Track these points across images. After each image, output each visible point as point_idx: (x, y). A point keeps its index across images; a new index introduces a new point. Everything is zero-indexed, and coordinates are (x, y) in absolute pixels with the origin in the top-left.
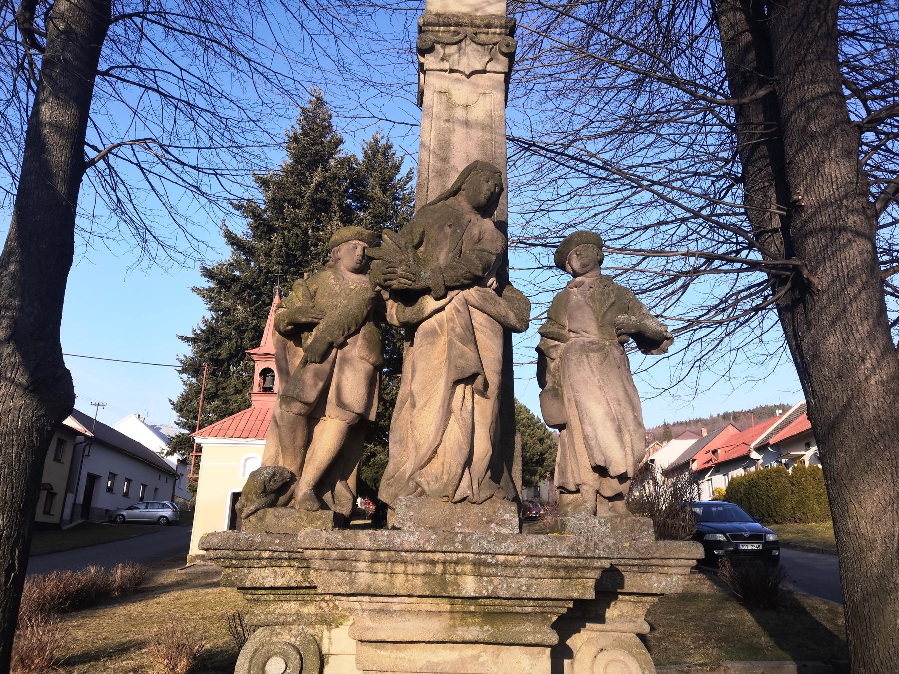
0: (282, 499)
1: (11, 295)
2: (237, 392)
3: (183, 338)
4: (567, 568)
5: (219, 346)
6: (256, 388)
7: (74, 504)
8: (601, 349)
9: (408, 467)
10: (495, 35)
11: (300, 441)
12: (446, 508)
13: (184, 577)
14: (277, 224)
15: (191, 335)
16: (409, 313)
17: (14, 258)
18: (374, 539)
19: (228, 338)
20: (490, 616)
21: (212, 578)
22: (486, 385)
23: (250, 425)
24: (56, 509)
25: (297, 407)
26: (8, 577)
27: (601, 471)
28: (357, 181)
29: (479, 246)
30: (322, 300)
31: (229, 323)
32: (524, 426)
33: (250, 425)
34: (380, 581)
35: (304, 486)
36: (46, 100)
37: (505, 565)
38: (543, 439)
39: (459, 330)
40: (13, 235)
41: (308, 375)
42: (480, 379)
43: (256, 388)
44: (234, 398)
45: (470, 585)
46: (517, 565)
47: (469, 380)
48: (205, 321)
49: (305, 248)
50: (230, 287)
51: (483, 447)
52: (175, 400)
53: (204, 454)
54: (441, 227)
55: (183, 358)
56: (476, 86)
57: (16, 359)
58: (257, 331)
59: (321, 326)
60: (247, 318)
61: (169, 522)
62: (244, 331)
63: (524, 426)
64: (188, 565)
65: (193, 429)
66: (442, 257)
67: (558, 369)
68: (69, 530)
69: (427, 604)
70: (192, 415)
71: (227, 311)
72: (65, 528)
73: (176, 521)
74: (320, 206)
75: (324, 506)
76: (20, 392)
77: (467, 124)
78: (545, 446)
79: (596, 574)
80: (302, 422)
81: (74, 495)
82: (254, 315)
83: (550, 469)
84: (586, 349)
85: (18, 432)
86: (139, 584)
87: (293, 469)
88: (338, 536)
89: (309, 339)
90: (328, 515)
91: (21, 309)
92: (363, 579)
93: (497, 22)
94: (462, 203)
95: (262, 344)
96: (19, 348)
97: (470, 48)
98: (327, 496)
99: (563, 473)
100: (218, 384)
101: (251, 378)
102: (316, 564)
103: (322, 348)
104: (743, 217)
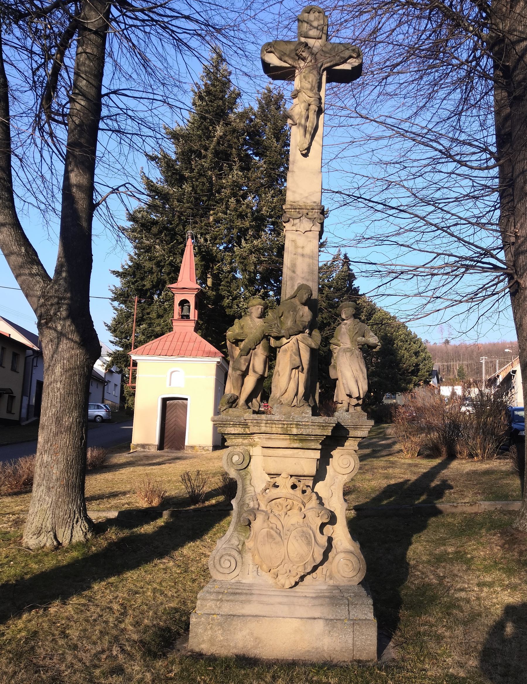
0: (234, 405)
1: (65, 291)
2: (159, 316)
3: (114, 272)
4: (323, 426)
5: (142, 279)
6: (176, 316)
7: (29, 405)
8: (351, 351)
9: (278, 395)
10: (316, 214)
11: (240, 385)
12: (289, 409)
13: (132, 459)
14: (187, 174)
15: (121, 270)
16: (278, 343)
17: (64, 269)
18: (266, 417)
19: (151, 272)
20: (301, 440)
21: (152, 460)
22: (303, 369)
23: (173, 345)
24: (16, 409)
25: (239, 372)
26: (81, 442)
27: (350, 396)
28: (254, 134)
29: (302, 319)
30: (246, 330)
31: (150, 259)
32: (401, 341)
33: (173, 345)
34: (268, 430)
35: (242, 400)
36: (72, 170)
37: (305, 425)
38: (419, 352)
39: (294, 351)
40: (61, 255)
41: (243, 360)
42: (300, 367)
43: (176, 316)
44: (157, 321)
45: (295, 431)
46: (308, 425)
47: (297, 368)
48: (131, 259)
49: (211, 195)
50: (150, 229)
51: (301, 390)
52: (110, 322)
53: (139, 368)
54: (289, 312)
55: (114, 289)
56: (307, 237)
57: (73, 328)
58: (172, 266)
59: (246, 340)
60: (164, 256)
61: (103, 420)
62: (163, 267)
63: (401, 341)
64: (131, 451)
65: (127, 347)
66: (289, 323)
67: (336, 357)
68: (27, 425)
69: (282, 437)
70: (124, 336)
71: (149, 249)
72: (24, 424)
73: (109, 420)
74: (222, 156)
75: (249, 408)
76: (76, 346)
77: (303, 255)
78: (420, 358)
79: (332, 428)
80: (241, 377)
81: (28, 398)
82: (170, 252)
83: (423, 378)
84: (345, 351)
85: (78, 368)
86: (102, 462)
87: (237, 394)
88: (256, 416)
89: (242, 345)
90: (251, 410)
91: (71, 299)
92: (263, 429)
93: (316, 207)
94: (296, 301)
95: (179, 279)
96: (73, 322)
97: (304, 219)
98: (250, 404)
99: (337, 396)
100: (143, 309)
101: (172, 306)
102: (249, 424)
103: (247, 350)
104: (499, 234)
